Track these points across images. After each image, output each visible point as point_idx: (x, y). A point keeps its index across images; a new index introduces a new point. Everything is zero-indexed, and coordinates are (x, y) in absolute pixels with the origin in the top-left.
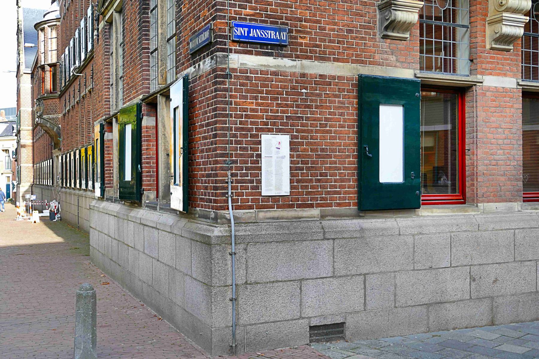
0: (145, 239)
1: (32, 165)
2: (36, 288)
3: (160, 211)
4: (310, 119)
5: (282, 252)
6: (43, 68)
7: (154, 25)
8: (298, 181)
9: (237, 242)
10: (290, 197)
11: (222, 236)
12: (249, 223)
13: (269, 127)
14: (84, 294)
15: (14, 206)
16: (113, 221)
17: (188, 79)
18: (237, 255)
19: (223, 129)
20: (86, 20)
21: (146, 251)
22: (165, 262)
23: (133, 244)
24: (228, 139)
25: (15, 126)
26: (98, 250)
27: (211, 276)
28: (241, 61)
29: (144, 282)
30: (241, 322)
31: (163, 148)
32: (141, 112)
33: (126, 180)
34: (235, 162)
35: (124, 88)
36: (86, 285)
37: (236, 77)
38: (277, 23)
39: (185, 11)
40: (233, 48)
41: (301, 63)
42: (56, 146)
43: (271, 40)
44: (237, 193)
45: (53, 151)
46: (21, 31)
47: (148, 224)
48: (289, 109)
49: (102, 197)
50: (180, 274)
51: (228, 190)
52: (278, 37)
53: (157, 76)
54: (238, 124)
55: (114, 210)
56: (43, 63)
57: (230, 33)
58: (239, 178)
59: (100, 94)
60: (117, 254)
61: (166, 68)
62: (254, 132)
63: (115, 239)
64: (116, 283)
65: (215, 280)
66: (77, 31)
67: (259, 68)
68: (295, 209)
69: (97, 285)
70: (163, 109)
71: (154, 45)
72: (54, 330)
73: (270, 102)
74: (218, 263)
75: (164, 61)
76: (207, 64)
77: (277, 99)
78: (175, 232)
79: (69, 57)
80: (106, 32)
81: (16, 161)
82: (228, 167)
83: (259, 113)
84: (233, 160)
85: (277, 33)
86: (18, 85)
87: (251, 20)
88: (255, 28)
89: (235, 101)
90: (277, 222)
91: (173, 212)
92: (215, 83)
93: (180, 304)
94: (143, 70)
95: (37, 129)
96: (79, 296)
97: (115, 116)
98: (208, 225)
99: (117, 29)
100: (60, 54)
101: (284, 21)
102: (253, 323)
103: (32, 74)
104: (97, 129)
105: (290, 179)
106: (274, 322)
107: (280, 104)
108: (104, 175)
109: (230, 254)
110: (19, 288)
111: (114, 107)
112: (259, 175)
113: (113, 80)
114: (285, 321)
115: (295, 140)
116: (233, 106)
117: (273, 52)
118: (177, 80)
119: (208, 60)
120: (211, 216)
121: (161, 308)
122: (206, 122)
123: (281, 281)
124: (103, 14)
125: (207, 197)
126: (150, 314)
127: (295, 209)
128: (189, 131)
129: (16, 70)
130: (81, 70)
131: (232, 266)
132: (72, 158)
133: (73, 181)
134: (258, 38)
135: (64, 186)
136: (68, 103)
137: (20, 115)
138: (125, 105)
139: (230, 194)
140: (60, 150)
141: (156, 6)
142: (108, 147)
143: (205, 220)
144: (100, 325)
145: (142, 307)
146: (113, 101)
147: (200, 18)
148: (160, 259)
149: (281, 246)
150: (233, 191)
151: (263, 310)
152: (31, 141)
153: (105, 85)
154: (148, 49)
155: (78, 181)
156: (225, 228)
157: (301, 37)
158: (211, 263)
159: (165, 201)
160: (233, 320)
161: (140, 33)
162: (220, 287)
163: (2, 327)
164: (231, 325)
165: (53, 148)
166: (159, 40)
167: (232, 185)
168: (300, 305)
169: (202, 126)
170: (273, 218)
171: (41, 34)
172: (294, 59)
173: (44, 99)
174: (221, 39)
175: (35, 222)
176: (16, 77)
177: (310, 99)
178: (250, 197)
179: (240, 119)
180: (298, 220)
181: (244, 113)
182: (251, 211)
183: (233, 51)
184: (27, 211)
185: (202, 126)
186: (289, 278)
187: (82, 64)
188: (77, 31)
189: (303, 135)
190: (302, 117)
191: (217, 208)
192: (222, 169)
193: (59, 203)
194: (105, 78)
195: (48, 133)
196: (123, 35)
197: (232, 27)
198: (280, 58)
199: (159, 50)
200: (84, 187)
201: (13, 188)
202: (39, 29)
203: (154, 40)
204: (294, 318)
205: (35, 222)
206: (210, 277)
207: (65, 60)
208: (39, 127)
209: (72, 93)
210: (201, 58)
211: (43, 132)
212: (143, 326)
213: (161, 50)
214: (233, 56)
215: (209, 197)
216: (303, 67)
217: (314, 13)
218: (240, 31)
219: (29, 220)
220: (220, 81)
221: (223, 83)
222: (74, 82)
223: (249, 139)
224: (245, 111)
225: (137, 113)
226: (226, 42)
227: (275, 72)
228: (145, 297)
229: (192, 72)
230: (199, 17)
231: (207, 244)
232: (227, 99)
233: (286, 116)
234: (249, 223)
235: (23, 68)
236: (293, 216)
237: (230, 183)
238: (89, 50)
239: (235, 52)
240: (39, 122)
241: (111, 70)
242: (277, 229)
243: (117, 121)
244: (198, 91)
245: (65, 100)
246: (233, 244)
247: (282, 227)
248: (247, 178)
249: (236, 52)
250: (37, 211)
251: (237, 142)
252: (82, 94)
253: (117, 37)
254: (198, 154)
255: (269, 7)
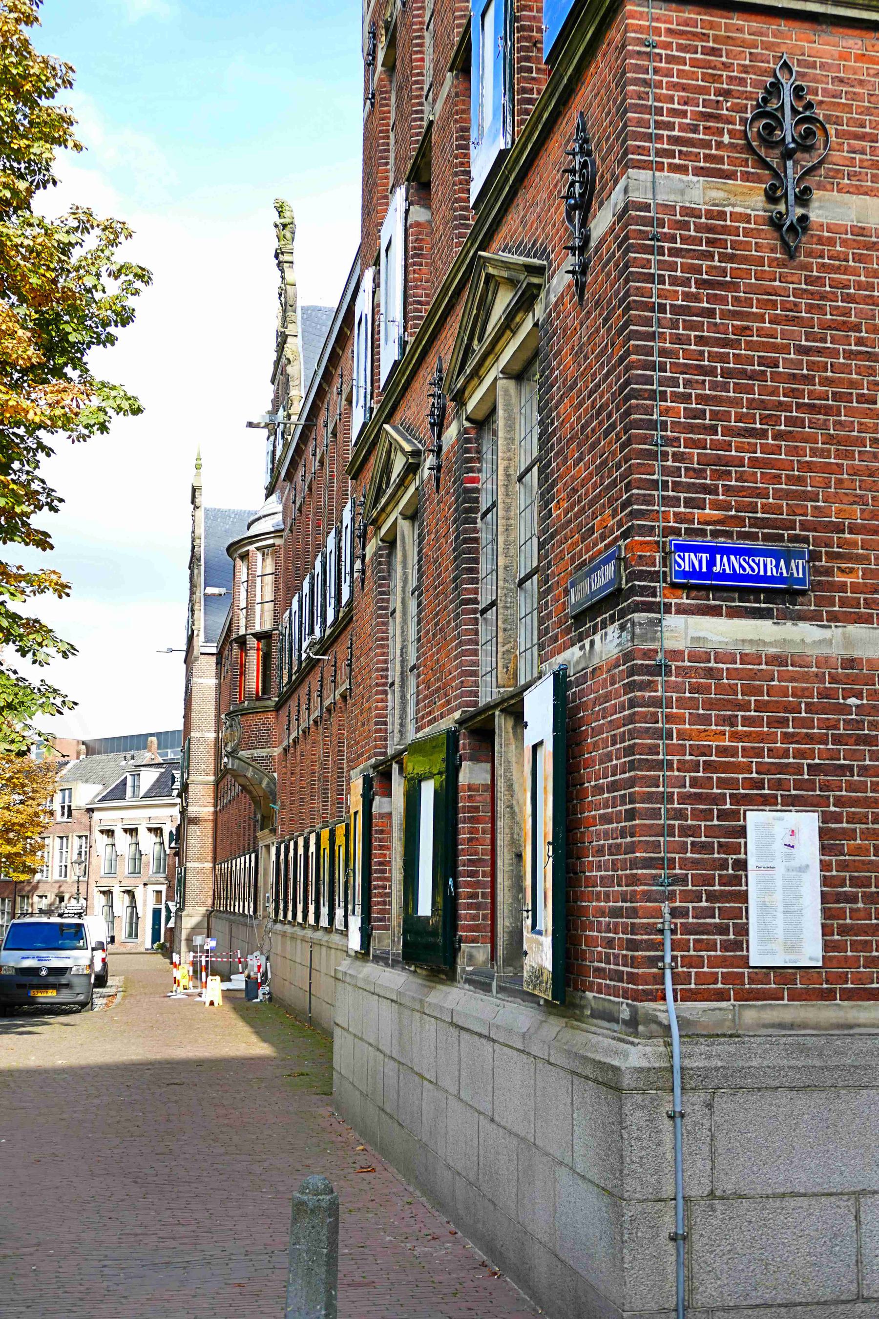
0: (463, 1065)
1: (211, 865)
2: (205, 1174)
3: (499, 996)
4: (871, 772)
5: (806, 1116)
6: (242, 642)
7: (489, 546)
8: (844, 930)
9: (688, 1086)
10: (823, 970)
11: (649, 1070)
12: (718, 1035)
13: (766, 791)
14: (310, 1204)
15: (168, 961)
16: (387, 1011)
17: (565, 676)
18: (687, 1120)
19: (649, 798)
20: (339, 533)
21: (463, 1095)
22: (508, 1126)
23: (433, 1074)
24: (662, 822)
25: (177, 774)
26: (352, 1083)
27: (621, 1171)
28: (692, 633)
29: (459, 1174)
30: (700, 1299)
31: (507, 839)
32: (457, 751)
33: (420, 914)
34: (683, 880)
35: (418, 693)
36: (317, 1180)
37: (683, 672)
38: (780, 538)
39: (559, 516)
40: (674, 601)
41: (844, 634)
42: (266, 821)
43: (765, 579)
44: (686, 960)
45: (259, 834)
46: (199, 560)
47: (471, 1027)
48: (817, 747)
49: (364, 953)
50: (545, 1159)
51: (663, 951)
52: (784, 571)
53: (494, 666)
54: (688, 784)
55: (392, 986)
56: (242, 632)
57: (665, 566)
58: (691, 920)
59: (366, 705)
60: (396, 1096)
61: (514, 648)
62: (728, 806)
63: (391, 1057)
64: (391, 1169)
65: (631, 1184)
66: (319, 558)
67: (737, 649)
68: (838, 1002)
69: (346, 1171)
70: (507, 745)
71: (489, 593)
72: (239, 1285)
73: (766, 729)
74: (638, 1138)
75: (510, 630)
76: (611, 641)
77: (784, 722)
78: (534, 1050)
79: (301, 617)
80: (380, 563)
81: (177, 854)
82: (664, 891)
83: (740, 759)
84: (676, 875)
85: (782, 562)
86: (188, 681)
87: (715, 534)
88: (727, 551)
89: (678, 730)
90: (790, 1036)
91: (530, 998)
92: (630, 687)
93: (545, 1239)
94: (464, 653)
95: (225, 780)
96: (299, 1207)
97: (398, 757)
98: (614, 1039)
99: (405, 556)
100: (280, 609)
101: (798, 532)
102: (731, 1304)
103: (219, 655)
104: (357, 785)
105: (824, 926)
106: (786, 1306)
107: (793, 735)
108: (370, 898)
109: (669, 1117)
110: (167, 1170)
111: (397, 735)
112: (741, 913)
113: (394, 674)
114: (818, 1303)
115: (833, 826)
116: (675, 741)
117: (772, 609)
118: (540, 678)
119: (613, 630)
120: (621, 1016)
121: (499, 1246)
122: (610, 779)
123: (805, 1195)
124: (376, 523)
125: (612, 966)
126: (470, 1257)
127: (838, 1002)
128: (569, 800)
129: (185, 648)
130: (325, 646)
131: (674, 1148)
132: (301, 851)
133: (300, 907)
134: (735, 576)
135: (281, 917)
136: (294, 723)
137: (189, 748)
138: (419, 735)
139: (668, 960)
140: (274, 831)
141: (494, 505)
142: (381, 832)
143: (606, 1024)
144: (349, 1280)
145: (451, 1238)
146: (393, 722)
147: (593, 534)
148: (496, 1118)
149: (801, 1101)
150: (675, 953)
151: (757, 1271)
152: (212, 809)
153: (377, 685)
154: (475, 601)
155: (312, 908)
156: (656, 1048)
157: (842, 571)
158: (622, 1138)
159: (511, 969)
160: (677, 1293)
161: (457, 567)
162: (643, 1201)
163: (123, 1269)
164: (673, 1306)
165: (259, 826)
166: (501, 581)
167: (674, 937)
168: (857, 1261)
169: (599, 790)
170: (781, 1026)
171: (242, 569)
172: (825, 623)
173: (244, 712)
174: (644, 580)
175: (212, 1003)
176: (185, 662)
177: (869, 722)
178: (720, 970)
179: (692, 774)
180: (846, 1032)
181: (702, 759)
182: (724, 1004)
183: (673, 609)
184: (196, 974)
185: (599, 790)
186: (826, 1186)
187: (328, 632)
188: (319, 558)
189: (854, 813)
190: (850, 768)
191: (637, 996)
192: (648, 897)
193: (268, 959)
194: (377, 670)
195: (249, 792)
196: (419, 570)
197: (671, 553)
198: (789, 623)
199: (500, 606)
200: (324, 922)
201: (168, 919)
202: (236, 555)
203: (489, 582)
204: (843, 1298)
205: (212, 1003)
206: (617, 1175)
207: (291, 624)
208: (229, 777)
209: (304, 700)
210: (596, 625)
211: (238, 788)
212: (452, 1290)
213: (505, 606)
214: (672, 621)
215: (616, 967)
216: (848, 641)
217: (872, 511)
218: (689, 561)
219: (198, 999)
220: (642, 681)
221: (649, 686)
222: (308, 673)
223: (716, 822)
224: (705, 755)
225: (448, 753)
226: (655, 587)
227: (779, 657)
228: (460, 1212)
229: (575, 659)
230: (592, 531)
231: (611, 1088)
232: (660, 725)
233: (809, 765)
234: (718, 1035)
235: (199, 640)
236: (834, 1021)
237: (668, 933)
238: (329, 623)
239: (678, 612)
240: (230, 766)
241: (390, 650)
242: (790, 1055)
243: (401, 770)
244: (590, 704)
245: (289, 716)
246: (678, 1090)
247: (804, 1050)
248: (713, 921)
249: (682, 610)
250: (218, 978)
251: (686, 831)
252: (327, 703)
253: (405, 574)
254: (590, 859)
255: (759, 501)
